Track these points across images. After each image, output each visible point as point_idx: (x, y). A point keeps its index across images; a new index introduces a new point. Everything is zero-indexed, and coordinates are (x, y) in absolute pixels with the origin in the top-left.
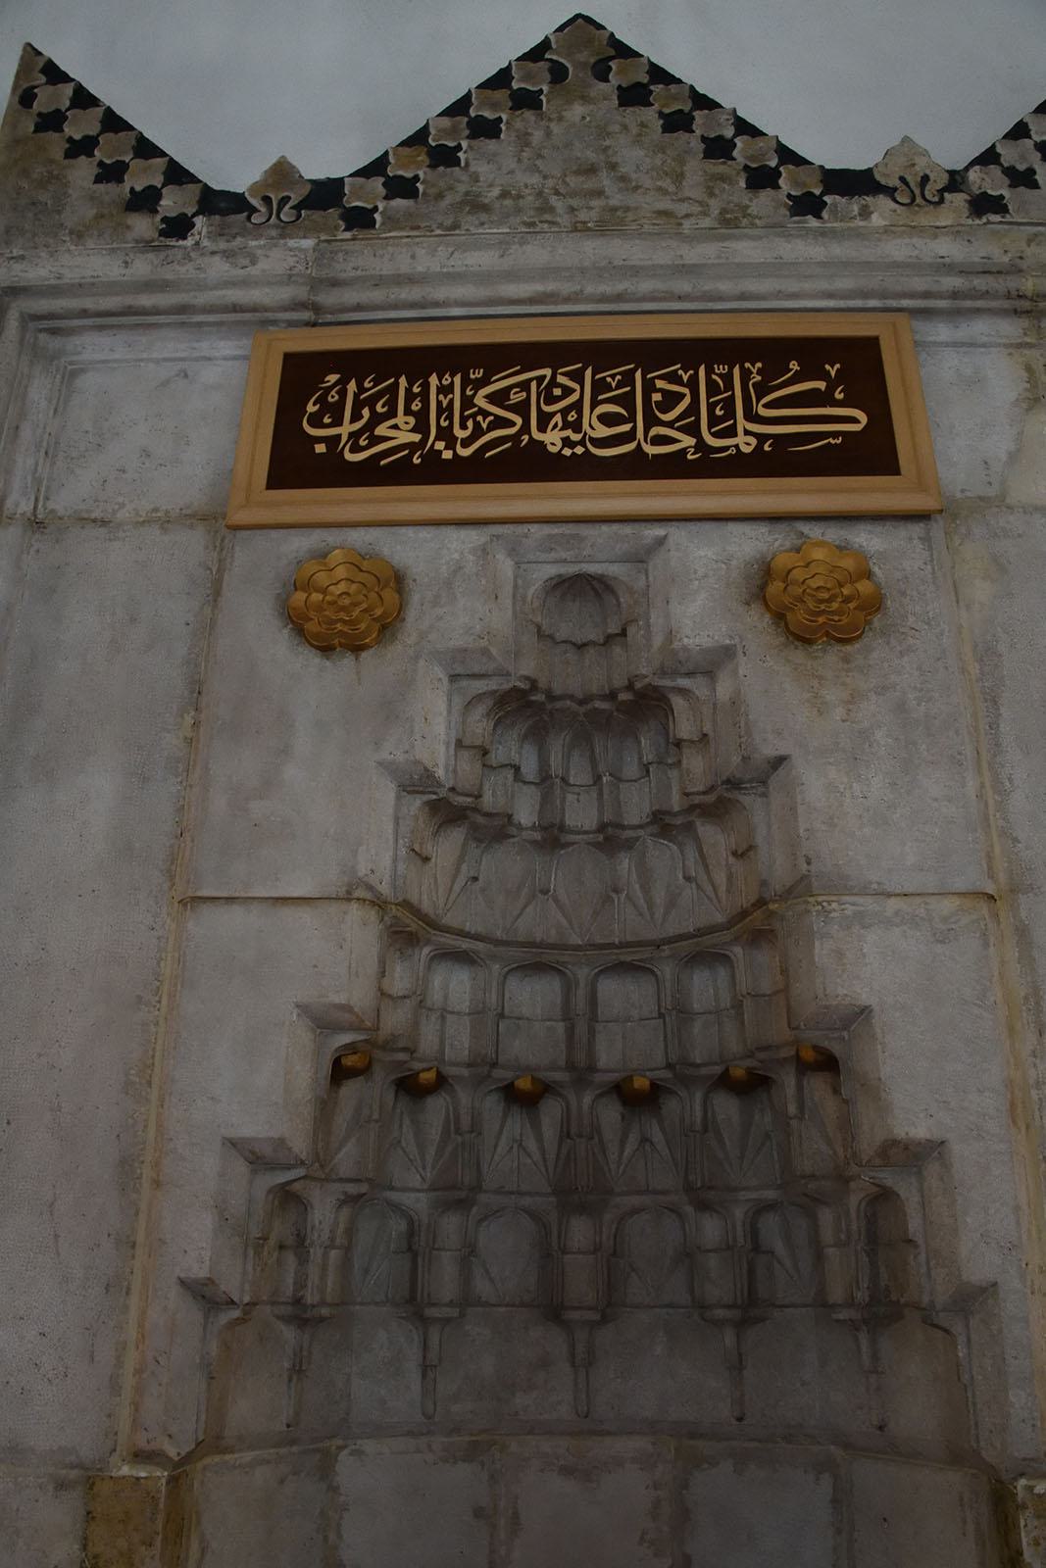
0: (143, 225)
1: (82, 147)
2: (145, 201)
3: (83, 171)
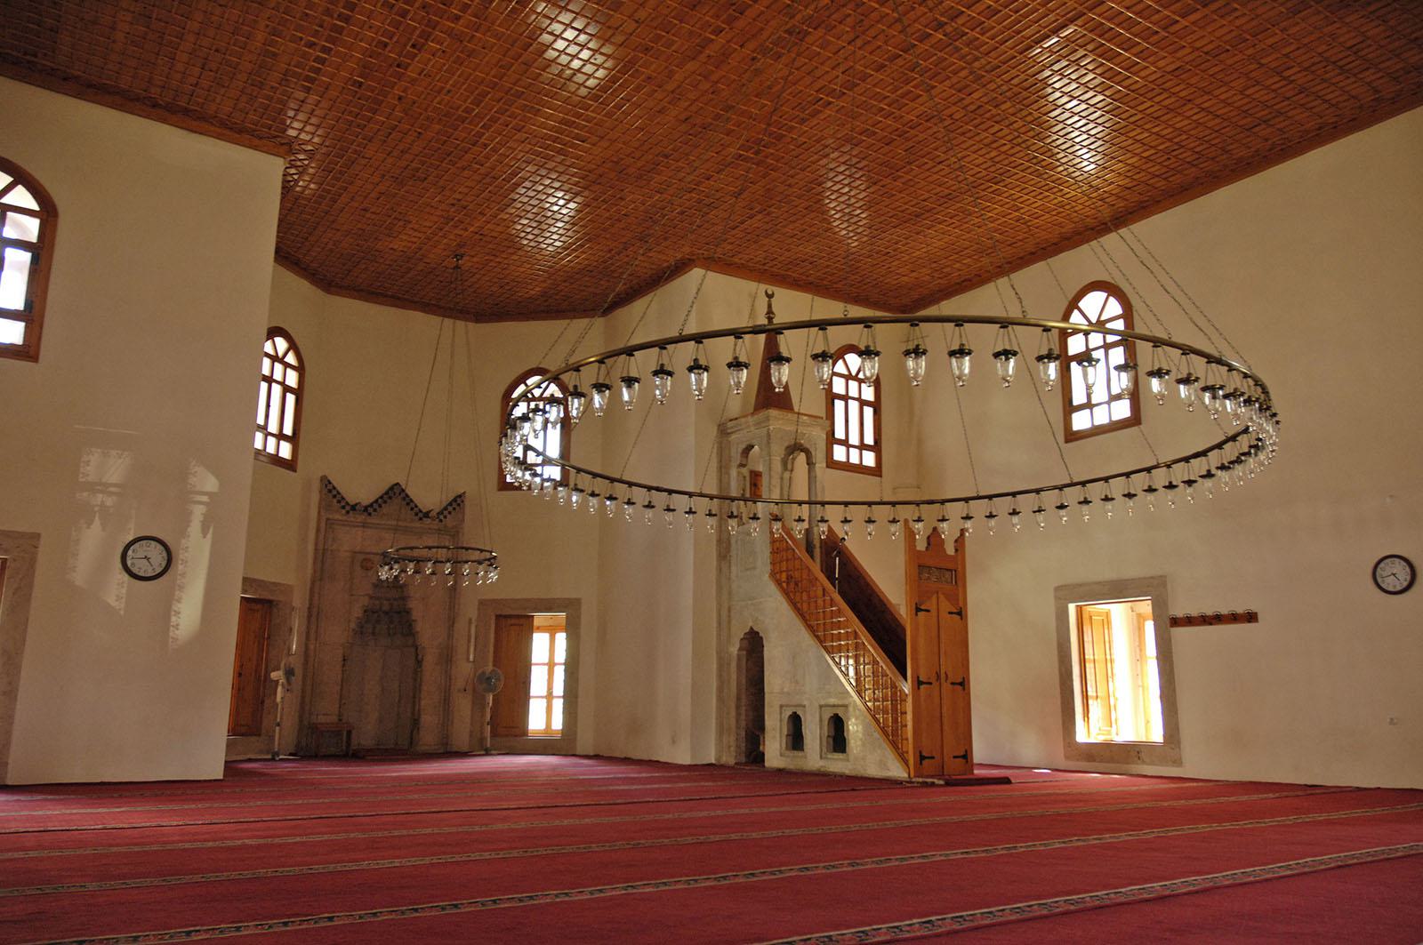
0: (344, 511)
1: (335, 496)
2: (343, 507)
3: (335, 501)
